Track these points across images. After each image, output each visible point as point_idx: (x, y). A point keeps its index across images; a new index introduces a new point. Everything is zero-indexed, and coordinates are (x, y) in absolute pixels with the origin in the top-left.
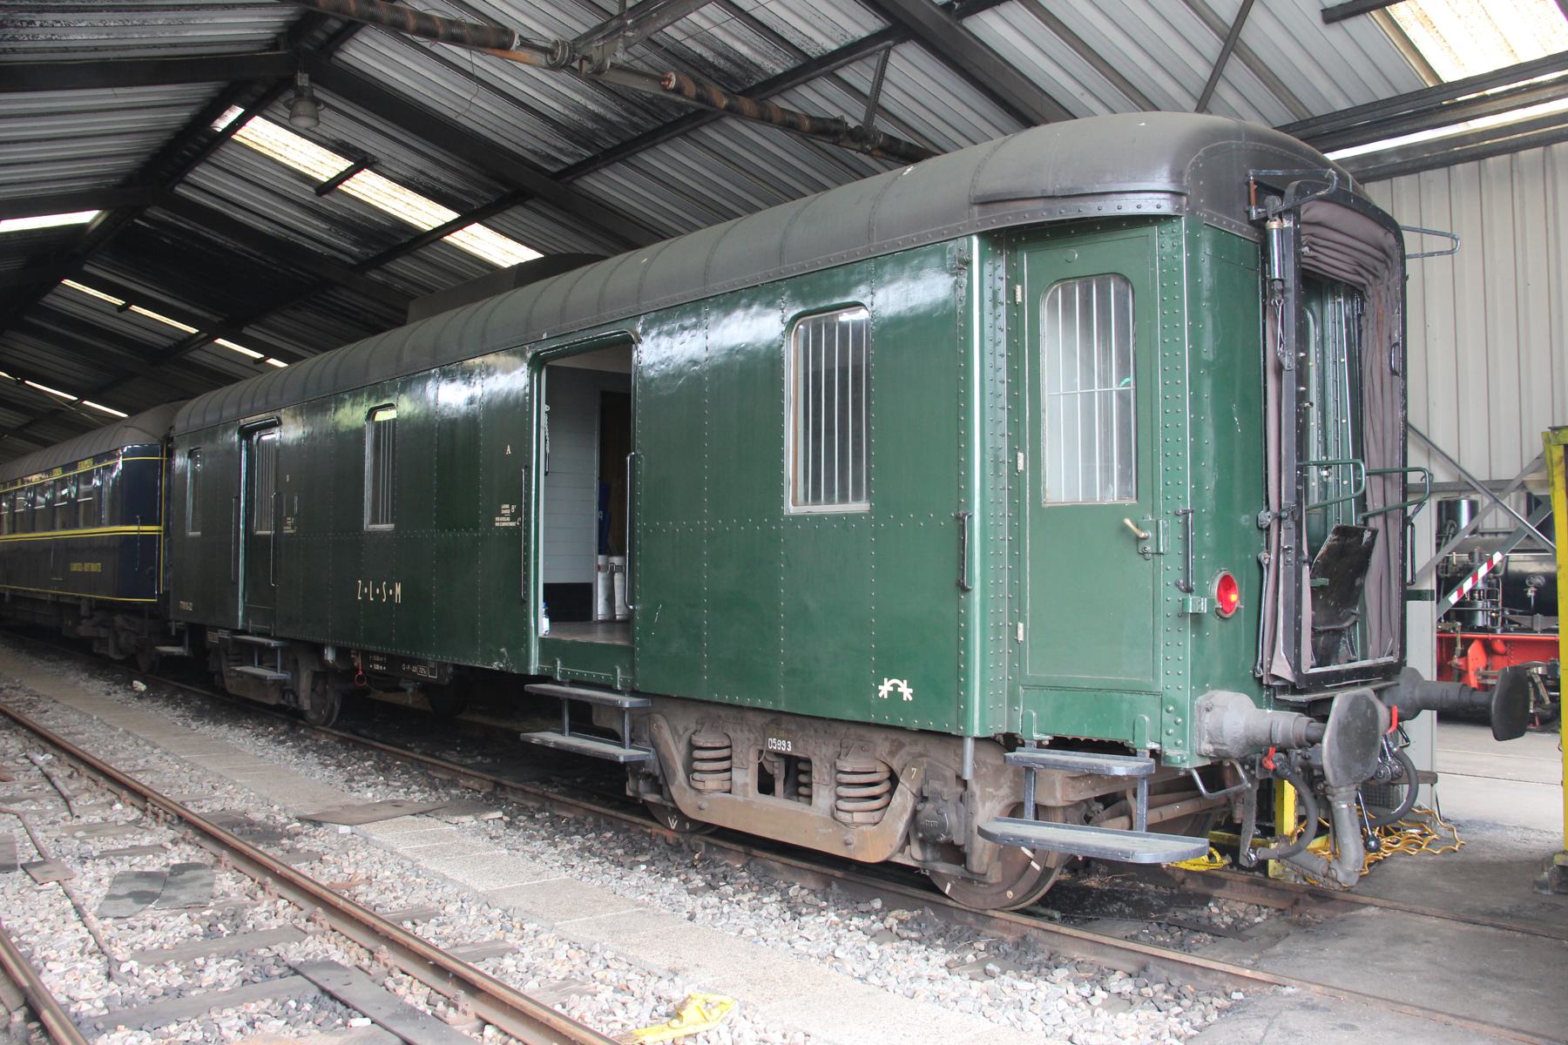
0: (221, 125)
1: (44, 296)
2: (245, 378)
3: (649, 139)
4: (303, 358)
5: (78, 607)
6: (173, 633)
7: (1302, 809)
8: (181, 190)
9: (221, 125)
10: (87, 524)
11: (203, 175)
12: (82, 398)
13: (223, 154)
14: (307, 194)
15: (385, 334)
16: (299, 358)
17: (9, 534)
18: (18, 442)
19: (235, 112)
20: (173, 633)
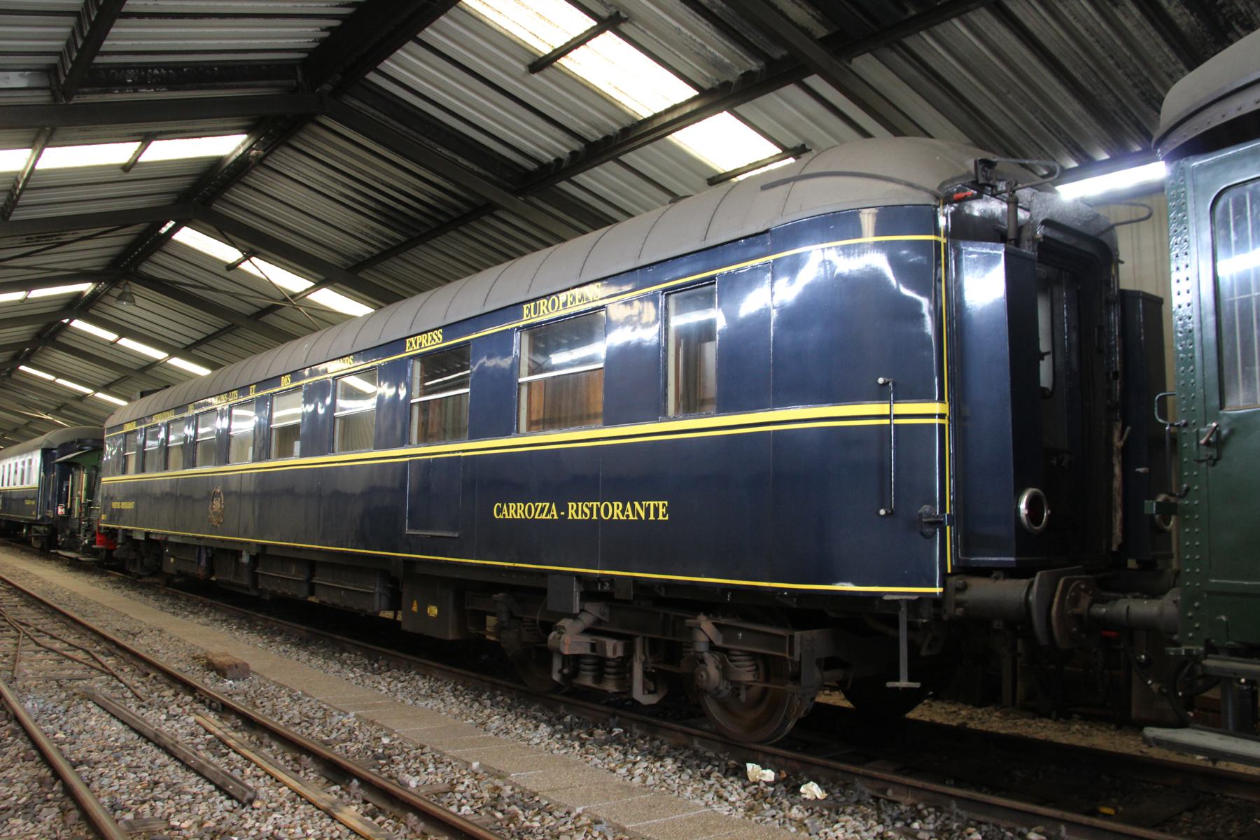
0: (164, 230)
1: (388, 52)
2: (174, 385)
3: (194, 344)
4: (223, 366)
5: (238, 554)
6: (917, 685)
7: (159, 564)
8: (372, 76)
9: (164, 230)
10: (346, 448)
11: (159, 257)
12: (96, 391)
13: (278, 158)
14: (109, 344)
15: (470, 277)
16: (381, 307)
17: (254, 461)
18: (27, 432)
19: (170, 224)
20: (917, 685)
